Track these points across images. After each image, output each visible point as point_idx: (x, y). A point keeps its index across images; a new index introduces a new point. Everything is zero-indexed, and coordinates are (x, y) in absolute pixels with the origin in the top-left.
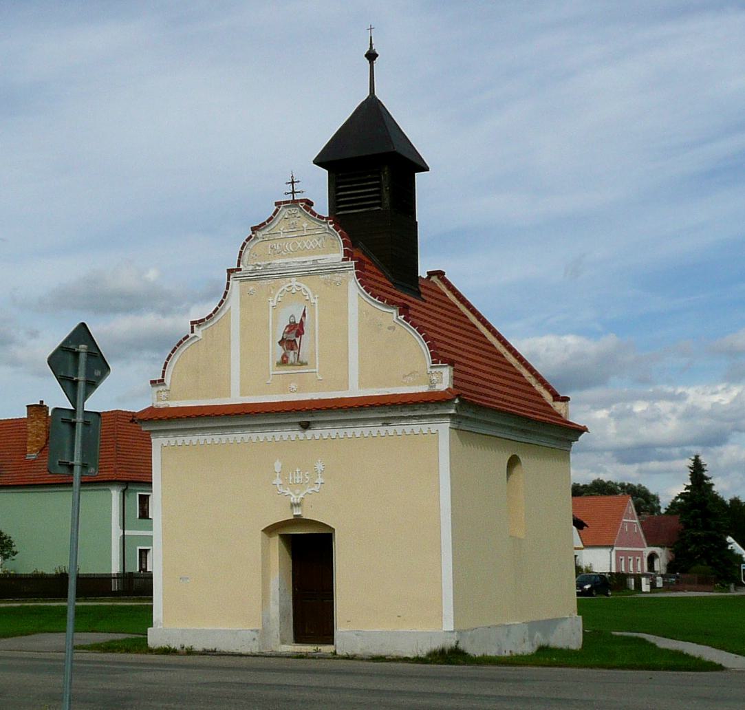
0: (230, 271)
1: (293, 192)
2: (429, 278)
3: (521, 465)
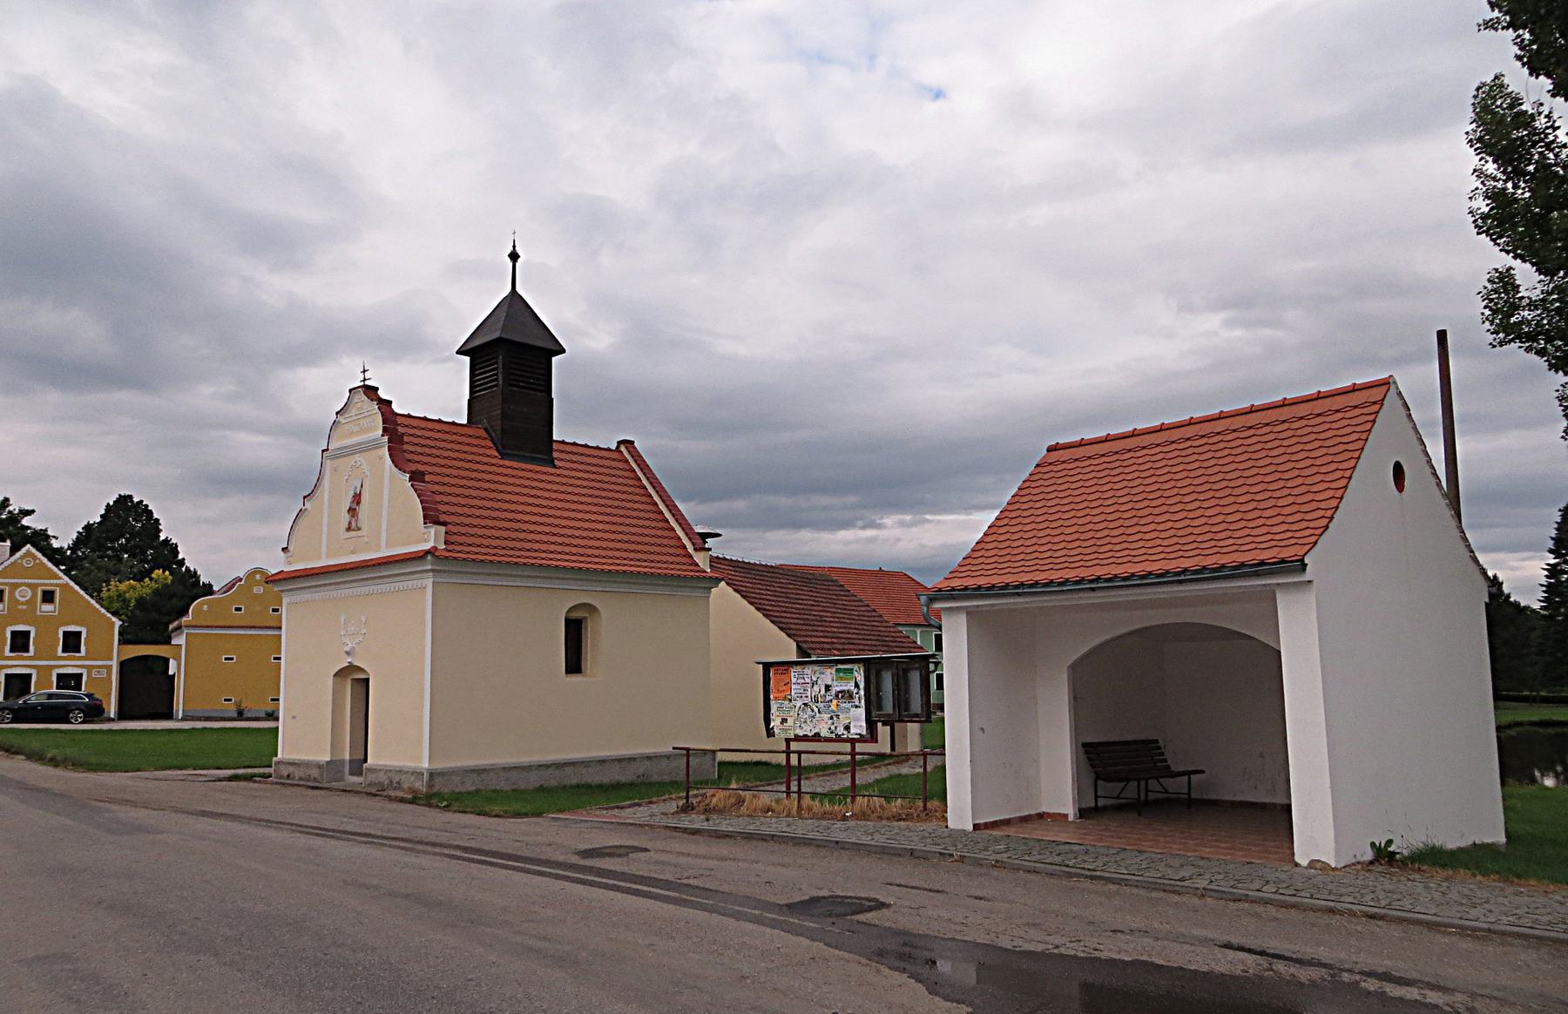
0: (323, 451)
1: (365, 380)
2: (618, 447)
3: (600, 616)
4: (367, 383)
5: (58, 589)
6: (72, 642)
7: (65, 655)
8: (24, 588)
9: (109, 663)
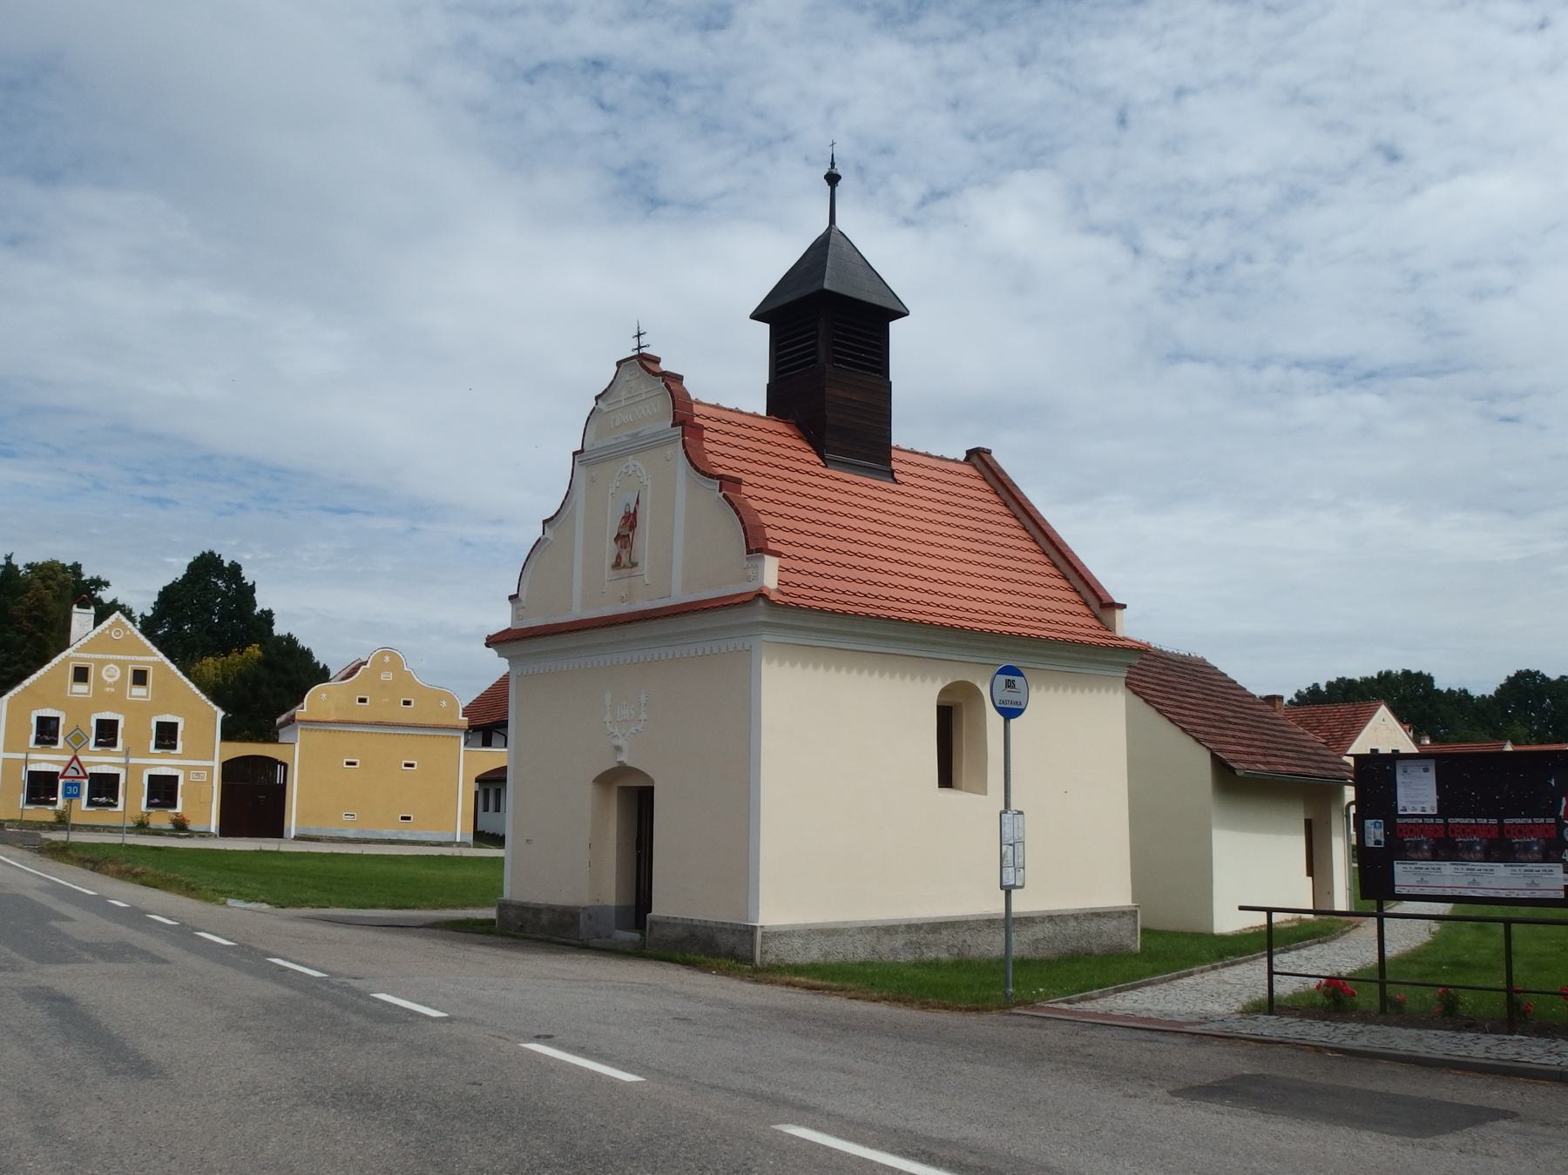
0: (575, 454)
1: (639, 347)
4: (643, 350)
5: (151, 667)
6: (166, 736)
7: (159, 751)
8: (112, 665)
9: (209, 763)
